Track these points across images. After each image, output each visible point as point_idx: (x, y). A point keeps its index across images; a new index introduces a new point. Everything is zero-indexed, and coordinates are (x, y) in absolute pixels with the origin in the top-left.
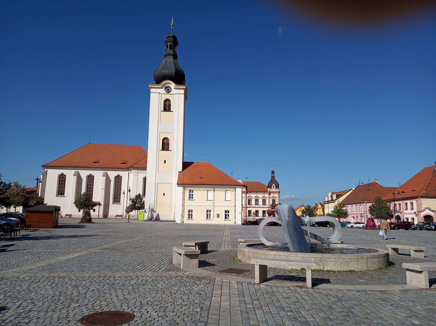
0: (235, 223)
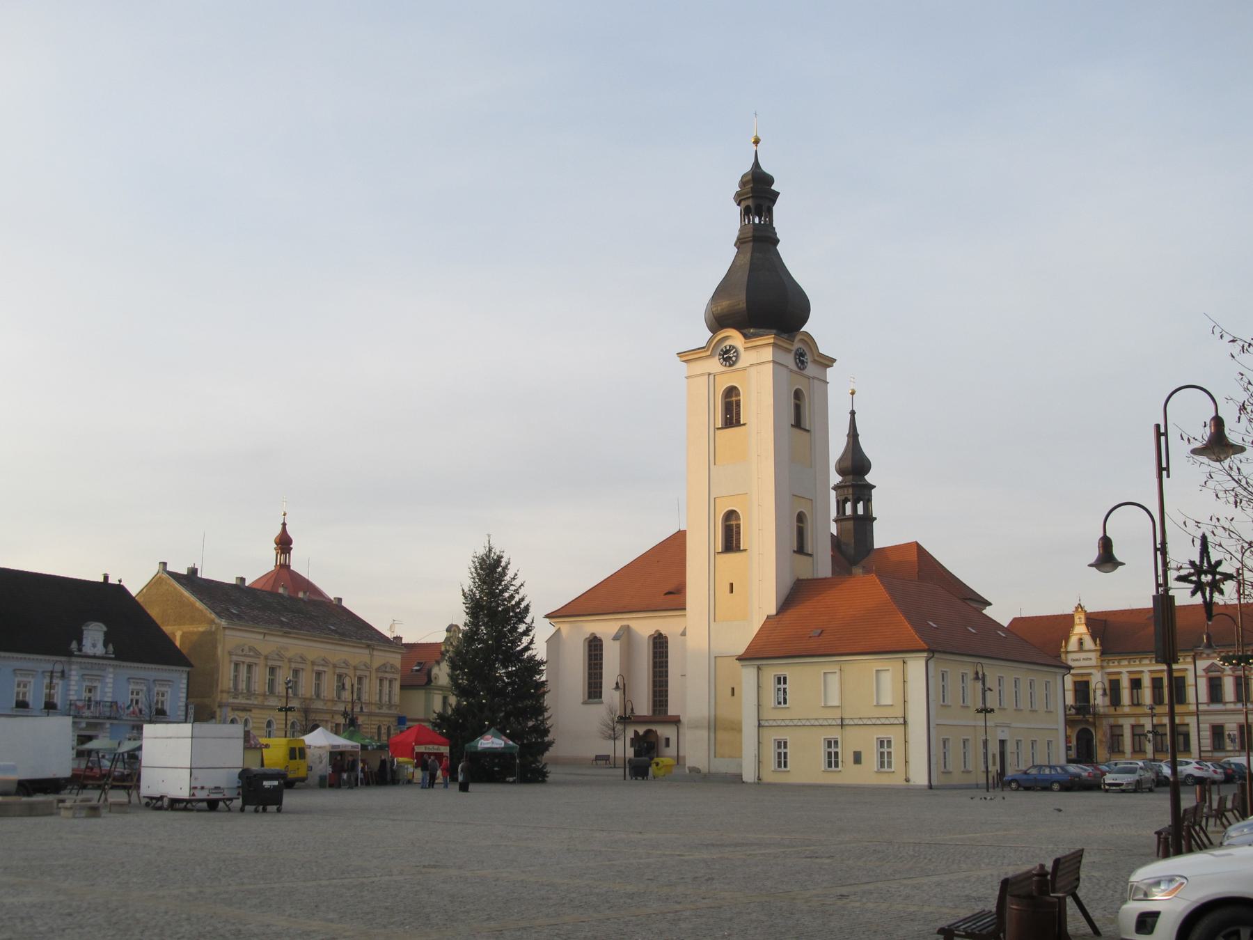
0: (907, 780)
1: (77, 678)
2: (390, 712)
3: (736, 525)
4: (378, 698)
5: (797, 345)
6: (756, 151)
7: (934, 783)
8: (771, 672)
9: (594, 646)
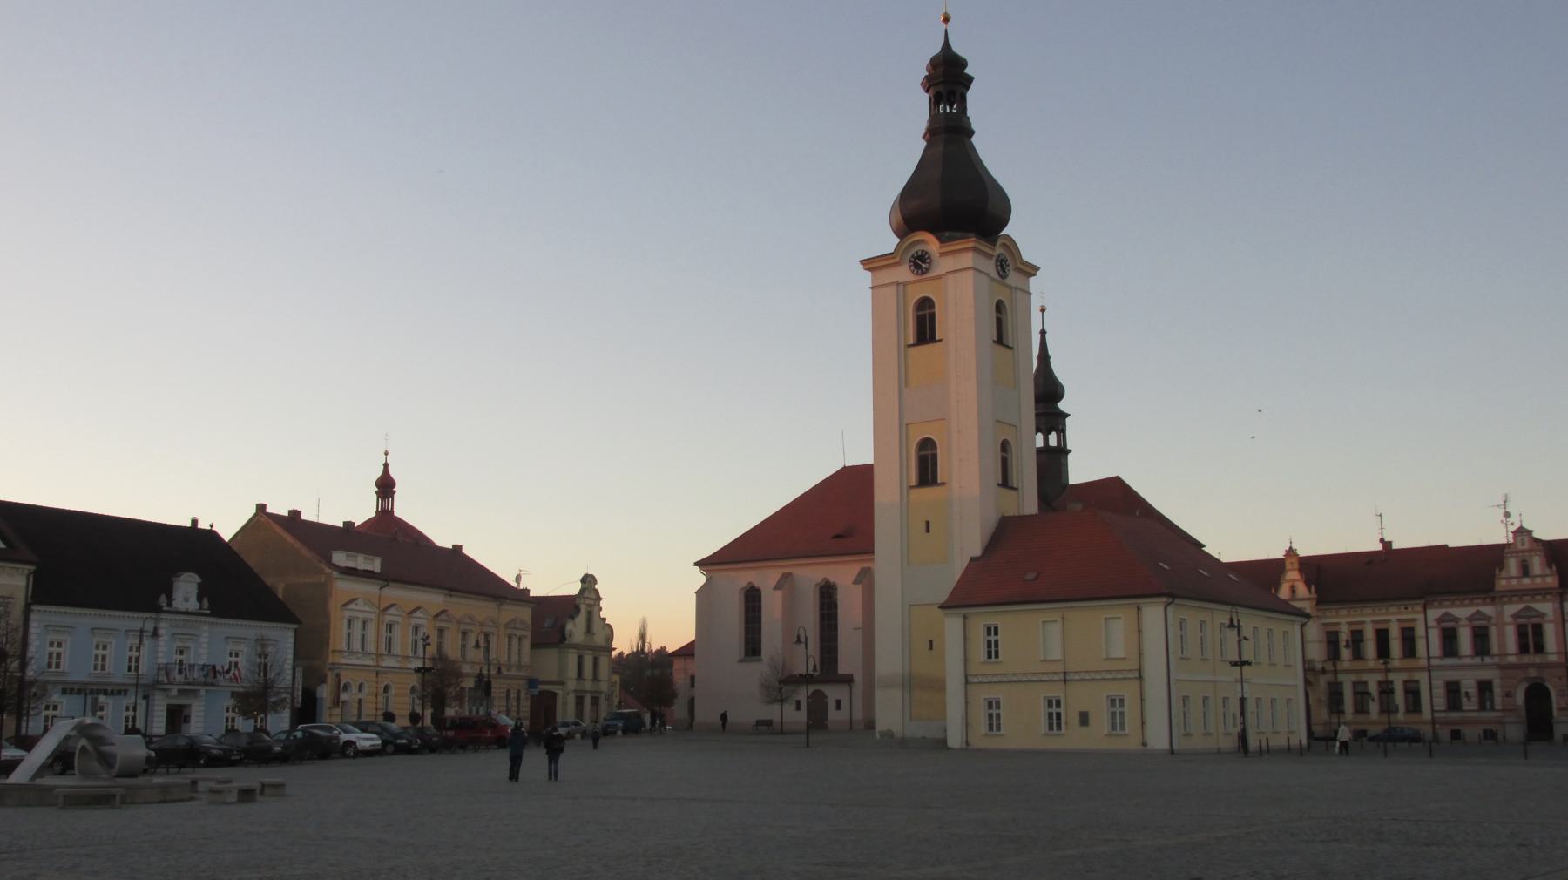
0: (1144, 744)
1: (165, 638)
2: (521, 674)
3: (932, 454)
4: (506, 658)
5: (998, 250)
6: (946, 30)
7: (1175, 747)
8: (981, 620)
9: (752, 598)
